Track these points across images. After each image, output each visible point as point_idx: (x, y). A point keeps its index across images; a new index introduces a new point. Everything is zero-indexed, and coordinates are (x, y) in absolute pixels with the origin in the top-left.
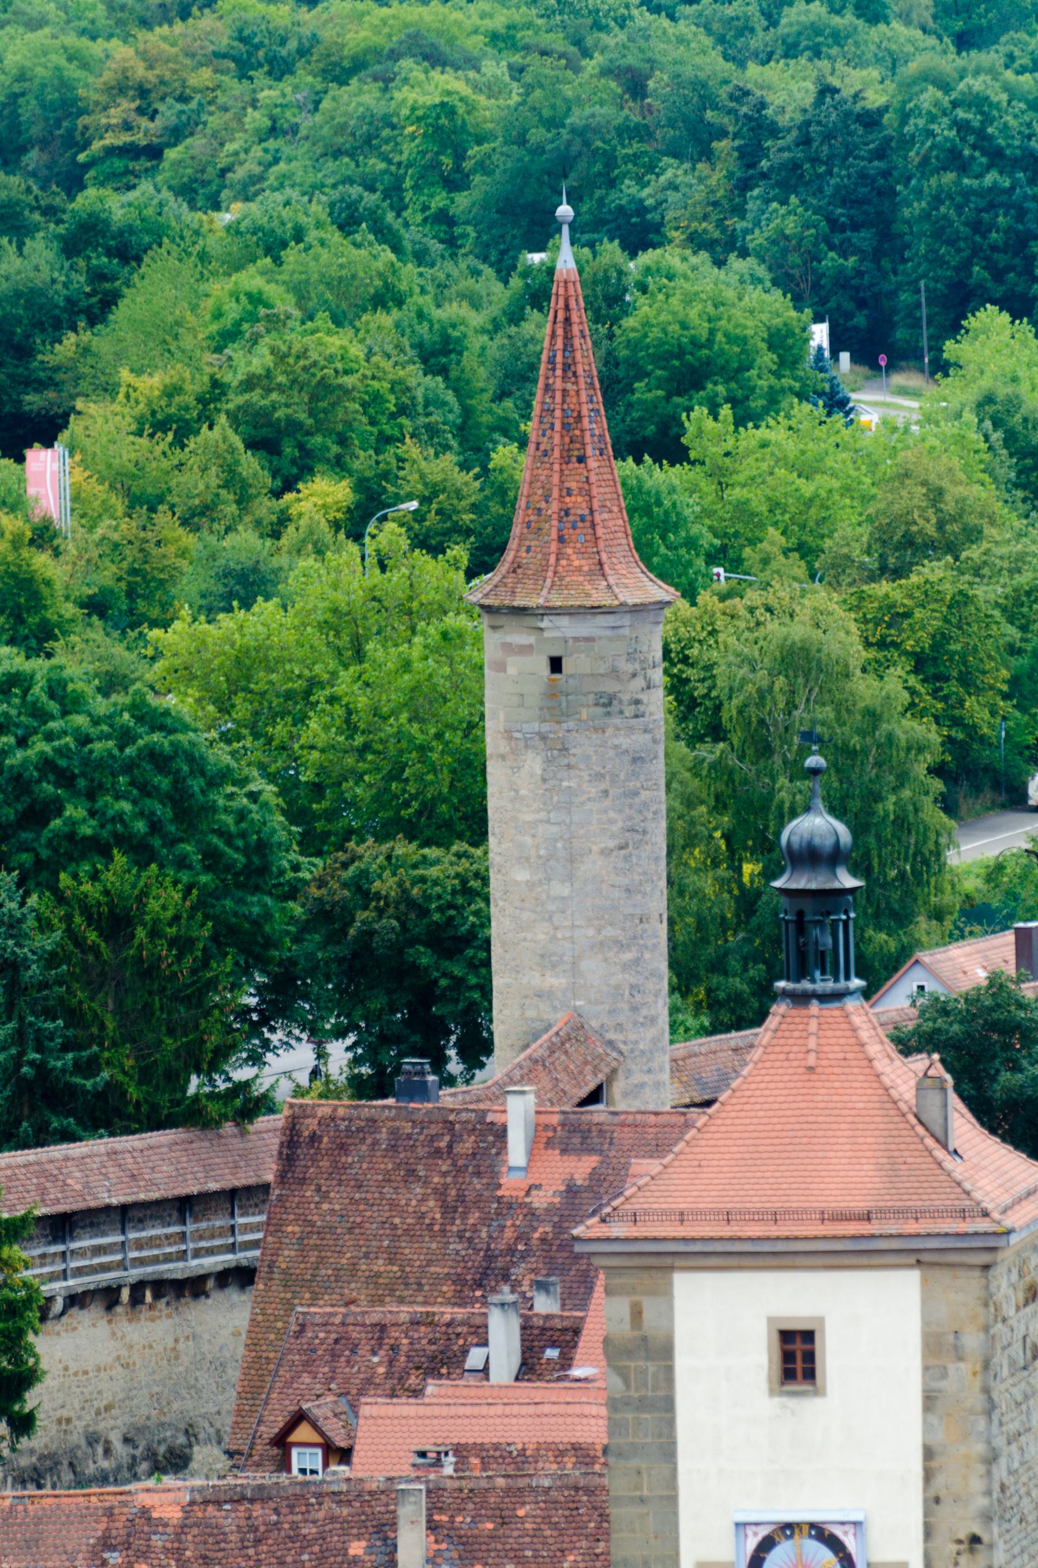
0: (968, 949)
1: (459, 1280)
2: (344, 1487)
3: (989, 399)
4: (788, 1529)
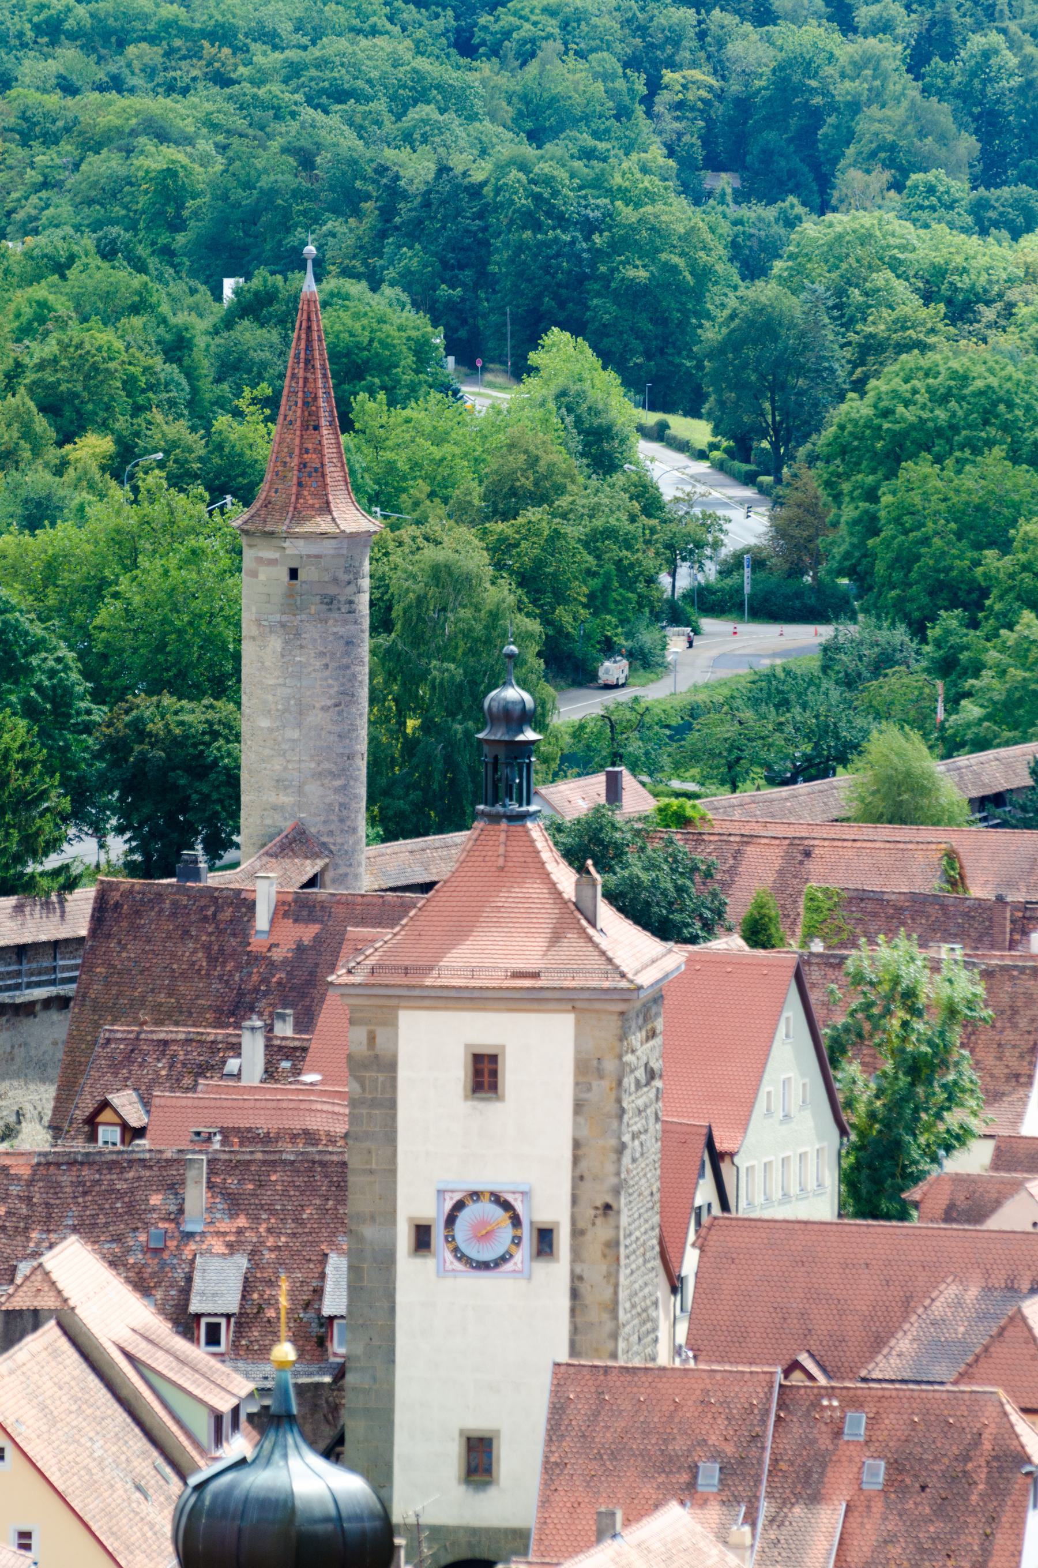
0: (572, 785)
1: (218, 1010)
2: (147, 1156)
3: (563, 393)
4: (475, 1195)
